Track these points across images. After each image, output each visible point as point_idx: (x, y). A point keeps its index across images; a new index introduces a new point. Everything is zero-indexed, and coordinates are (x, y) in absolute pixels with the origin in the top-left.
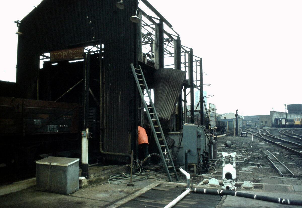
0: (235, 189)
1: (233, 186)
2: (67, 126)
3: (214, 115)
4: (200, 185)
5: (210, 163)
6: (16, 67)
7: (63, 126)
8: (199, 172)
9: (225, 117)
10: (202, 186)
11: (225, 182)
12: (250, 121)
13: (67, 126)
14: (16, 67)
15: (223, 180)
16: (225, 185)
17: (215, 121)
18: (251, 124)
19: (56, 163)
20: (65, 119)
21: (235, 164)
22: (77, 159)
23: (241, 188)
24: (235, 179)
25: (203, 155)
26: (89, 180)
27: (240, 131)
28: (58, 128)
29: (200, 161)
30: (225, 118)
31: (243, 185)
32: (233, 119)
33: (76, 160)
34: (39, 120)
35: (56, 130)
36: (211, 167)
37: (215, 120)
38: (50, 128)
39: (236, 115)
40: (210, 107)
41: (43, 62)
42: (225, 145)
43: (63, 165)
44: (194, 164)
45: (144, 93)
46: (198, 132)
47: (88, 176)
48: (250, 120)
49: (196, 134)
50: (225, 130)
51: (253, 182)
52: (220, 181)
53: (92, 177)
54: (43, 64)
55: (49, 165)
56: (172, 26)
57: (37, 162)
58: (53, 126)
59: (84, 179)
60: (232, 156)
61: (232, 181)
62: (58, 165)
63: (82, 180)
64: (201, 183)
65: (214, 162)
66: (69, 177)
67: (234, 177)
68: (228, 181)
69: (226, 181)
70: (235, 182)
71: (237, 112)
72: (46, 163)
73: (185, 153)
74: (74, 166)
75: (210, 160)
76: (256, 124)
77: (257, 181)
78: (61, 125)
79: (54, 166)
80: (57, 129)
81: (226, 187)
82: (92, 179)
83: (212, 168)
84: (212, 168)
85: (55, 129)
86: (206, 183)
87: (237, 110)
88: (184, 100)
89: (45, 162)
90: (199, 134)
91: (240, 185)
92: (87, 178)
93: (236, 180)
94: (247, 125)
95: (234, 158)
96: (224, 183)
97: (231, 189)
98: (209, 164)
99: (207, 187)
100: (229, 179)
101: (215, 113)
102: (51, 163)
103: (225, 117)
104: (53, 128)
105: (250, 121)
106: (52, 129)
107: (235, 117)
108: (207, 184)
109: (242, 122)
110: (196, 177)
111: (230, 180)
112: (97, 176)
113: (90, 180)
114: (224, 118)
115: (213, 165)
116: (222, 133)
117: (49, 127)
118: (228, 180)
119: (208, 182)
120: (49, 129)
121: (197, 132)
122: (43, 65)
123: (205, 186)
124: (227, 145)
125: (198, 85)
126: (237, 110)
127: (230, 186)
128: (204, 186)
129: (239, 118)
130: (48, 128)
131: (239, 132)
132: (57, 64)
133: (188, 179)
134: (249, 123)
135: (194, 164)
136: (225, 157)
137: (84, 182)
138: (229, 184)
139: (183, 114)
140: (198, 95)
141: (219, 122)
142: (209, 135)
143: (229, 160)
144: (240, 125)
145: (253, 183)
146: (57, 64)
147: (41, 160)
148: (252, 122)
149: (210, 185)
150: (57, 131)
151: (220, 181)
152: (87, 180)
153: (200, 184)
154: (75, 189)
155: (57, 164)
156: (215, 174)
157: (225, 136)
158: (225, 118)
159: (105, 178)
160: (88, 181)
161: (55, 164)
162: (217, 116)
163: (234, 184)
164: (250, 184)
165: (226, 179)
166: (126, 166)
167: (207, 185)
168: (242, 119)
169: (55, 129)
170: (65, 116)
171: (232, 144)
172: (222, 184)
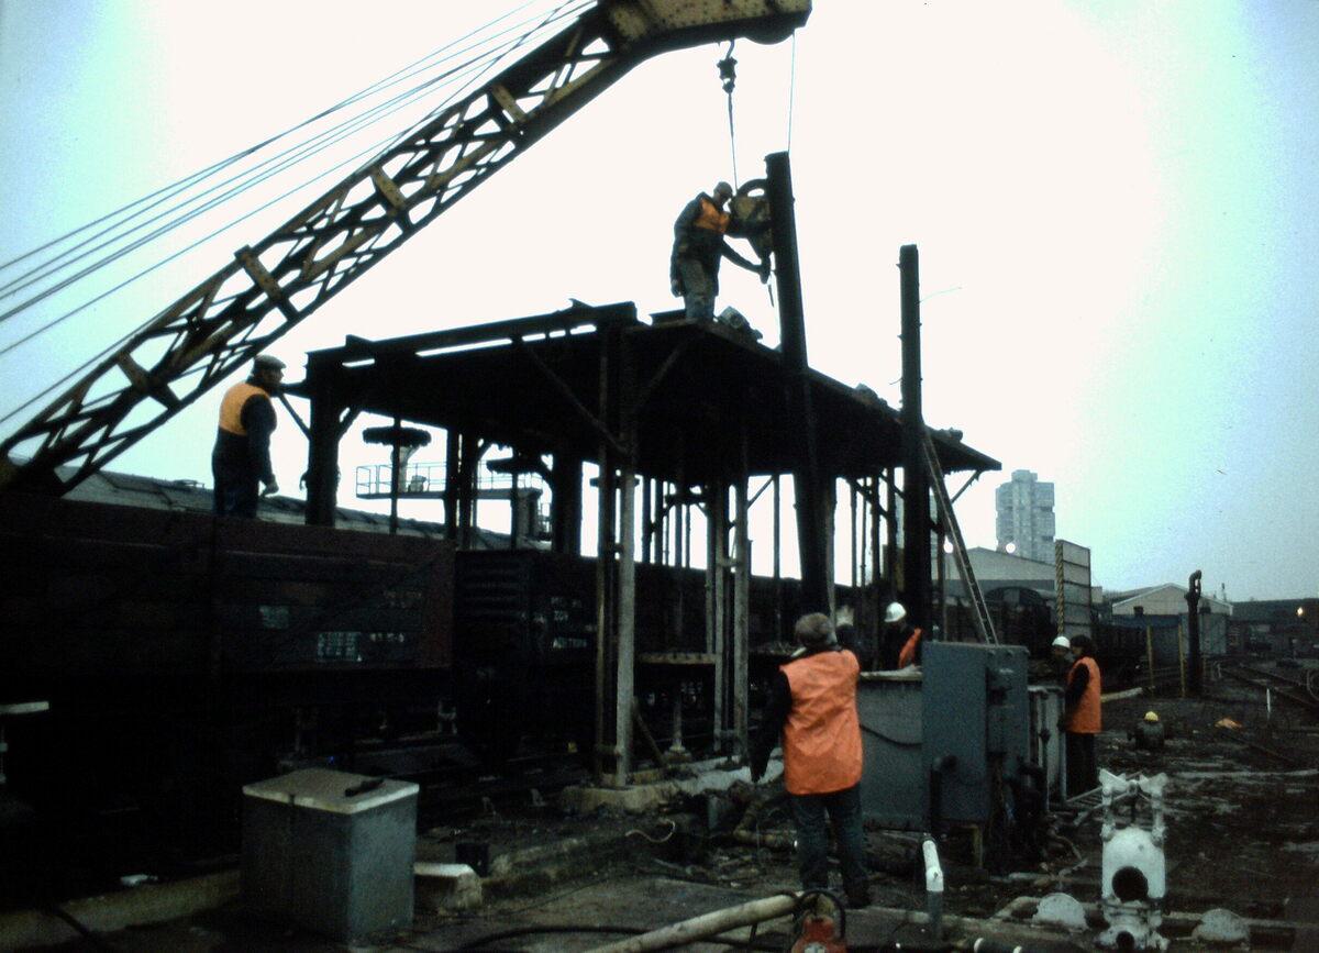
0: (1158, 946)
1: (1151, 933)
2: (401, 636)
3: (1083, 599)
4: (998, 921)
5: (1054, 821)
6: (900, 337)
7: (384, 636)
8: (998, 864)
9: (1136, 608)
10: (1006, 930)
11: (1112, 910)
12: (1263, 629)
13: (401, 636)
14: (900, 337)
15: (1105, 901)
16: (1112, 928)
17: (1090, 625)
18: (1269, 641)
19: (310, 796)
20: (393, 604)
21: (1159, 830)
22: (406, 786)
23: (1188, 942)
24: (1159, 900)
25: (1016, 786)
26: (487, 880)
27: (1212, 672)
28: (361, 644)
29: (1003, 810)
30: (1139, 610)
31: (1201, 930)
32: (1181, 614)
33: (399, 789)
34: (283, 611)
35: (352, 654)
36: (1054, 840)
37: (1088, 621)
38: (326, 645)
39: (1193, 595)
40: (1063, 561)
41: (307, 357)
42: (1133, 740)
43: (338, 806)
44: (974, 826)
45: (750, 498)
46: (990, 677)
47: (485, 865)
48: (1264, 623)
49: (984, 683)
50: (1139, 670)
51: (1253, 912)
52: (1093, 906)
53: (502, 865)
54: (921, 328)
55: (286, 805)
56: (1052, 485)
57: (249, 791)
58: (340, 634)
59: (468, 876)
60: (1145, 790)
61: (1145, 911)
62: (321, 806)
63: (460, 877)
64: (1005, 913)
65: (1069, 819)
66: (362, 864)
67: (1157, 887)
68: (1129, 908)
69: (1116, 907)
70: (1159, 912)
71: (1196, 584)
72: (279, 797)
73: (932, 771)
74: (385, 817)
75: (1052, 809)
76: (1294, 641)
77: (1277, 912)
78: (375, 632)
79: (304, 811)
80: (358, 652)
81: (1116, 934)
82: (503, 878)
83: (1060, 846)
84: (1060, 846)
85: (350, 650)
86: (1026, 914)
87: (1197, 575)
88: (882, 517)
89: (275, 789)
90: (995, 686)
91: (1188, 928)
92: (482, 871)
93: (1167, 904)
94: (1248, 646)
95: (1158, 799)
96: (1107, 918)
97: (1143, 947)
98: (1047, 826)
99: (1027, 934)
100: (1131, 899)
101: (1089, 587)
102: (292, 797)
103: (1136, 608)
104: (341, 645)
105: (1263, 629)
106: (334, 649)
107: (1184, 608)
108: (1028, 920)
109: (1222, 632)
110: (982, 887)
111: (1137, 904)
112: (529, 865)
113: (495, 878)
114: (1132, 612)
115: (1062, 831)
116: (1126, 681)
117: (323, 640)
118: (1128, 904)
119: (1036, 911)
120: (324, 650)
121: (987, 676)
122: (305, 370)
123: (1022, 930)
124: (1142, 740)
125: (509, 485)
126: (1197, 575)
127: (1137, 932)
128: (1017, 926)
129: (1206, 610)
130: (320, 645)
131: (1208, 677)
132: (371, 361)
133: (932, 893)
134: (1257, 634)
135: (974, 822)
136: (1115, 793)
137: (469, 888)
138: (1129, 920)
139: (931, 590)
140: (1011, 501)
141: (1109, 629)
142: (1045, 691)
143: (1133, 810)
144: (1213, 643)
145: (1248, 922)
146: (371, 361)
147: (271, 782)
148: (1273, 631)
149: (1042, 923)
150: (359, 659)
151: (1093, 906)
152: (481, 881)
153: (999, 918)
154: (393, 921)
155: (314, 803)
156: (1080, 872)
157: (1139, 695)
158: (1139, 610)
159: (560, 874)
160: (484, 886)
161: (307, 802)
162: (1097, 600)
163: (1156, 921)
164: (1233, 925)
165: (1118, 901)
166: (657, 823)
167: (1029, 924)
168: (1226, 616)
169: (350, 650)
170: (392, 594)
171: (1169, 737)
172: (1097, 923)
